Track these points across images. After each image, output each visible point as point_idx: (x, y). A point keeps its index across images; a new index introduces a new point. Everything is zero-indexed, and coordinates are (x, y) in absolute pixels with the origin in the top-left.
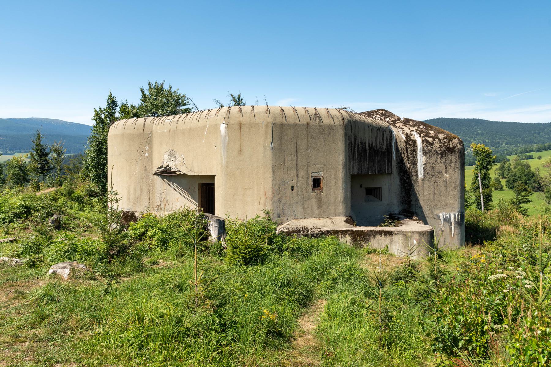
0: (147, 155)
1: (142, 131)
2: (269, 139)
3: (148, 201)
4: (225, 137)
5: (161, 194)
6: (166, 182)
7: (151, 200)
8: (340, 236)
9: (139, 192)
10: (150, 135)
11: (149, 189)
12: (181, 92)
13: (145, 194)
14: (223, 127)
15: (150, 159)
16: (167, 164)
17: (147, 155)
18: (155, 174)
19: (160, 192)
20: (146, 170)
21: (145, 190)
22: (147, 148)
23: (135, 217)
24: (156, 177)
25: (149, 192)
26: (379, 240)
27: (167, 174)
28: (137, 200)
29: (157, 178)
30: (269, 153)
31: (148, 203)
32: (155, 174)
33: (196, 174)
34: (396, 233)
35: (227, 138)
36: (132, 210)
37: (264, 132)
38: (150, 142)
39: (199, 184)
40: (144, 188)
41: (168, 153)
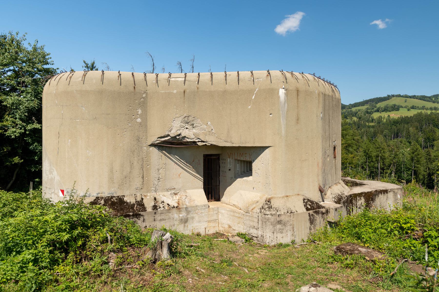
0: (139, 120)
1: (132, 89)
2: (321, 109)
3: (141, 180)
4: (285, 104)
5: (158, 170)
6: (165, 155)
7: (146, 179)
8: (358, 198)
9: (128, 169)
10: (144, 96)
11: (142, 165)
12: (46, 50)
13: (136, 172)
14: (282, 92)
15: (144, 125)
16: (179, 132)
17: (139, 120)
18: (152, 145)
19: (157, 167)
20: (138, 139)
21: (137, 166)
22: (140, 112)
23: (127, 203)
24: (152, 148)
25: (142, 168)
26: (380, 198)
27: (172, 145)
28: (126, 179)
29: (154, 150)
30: (320, 123)
31: (141, 183)
32: (152, 145)
33: (234, 145)
34: (389, 190)
35: (286, 105)
36: (119, 194)
37: (317, 101)
38: (144, 104)
39: (204, 155)
40: (135, 163)
41: (180, 119)
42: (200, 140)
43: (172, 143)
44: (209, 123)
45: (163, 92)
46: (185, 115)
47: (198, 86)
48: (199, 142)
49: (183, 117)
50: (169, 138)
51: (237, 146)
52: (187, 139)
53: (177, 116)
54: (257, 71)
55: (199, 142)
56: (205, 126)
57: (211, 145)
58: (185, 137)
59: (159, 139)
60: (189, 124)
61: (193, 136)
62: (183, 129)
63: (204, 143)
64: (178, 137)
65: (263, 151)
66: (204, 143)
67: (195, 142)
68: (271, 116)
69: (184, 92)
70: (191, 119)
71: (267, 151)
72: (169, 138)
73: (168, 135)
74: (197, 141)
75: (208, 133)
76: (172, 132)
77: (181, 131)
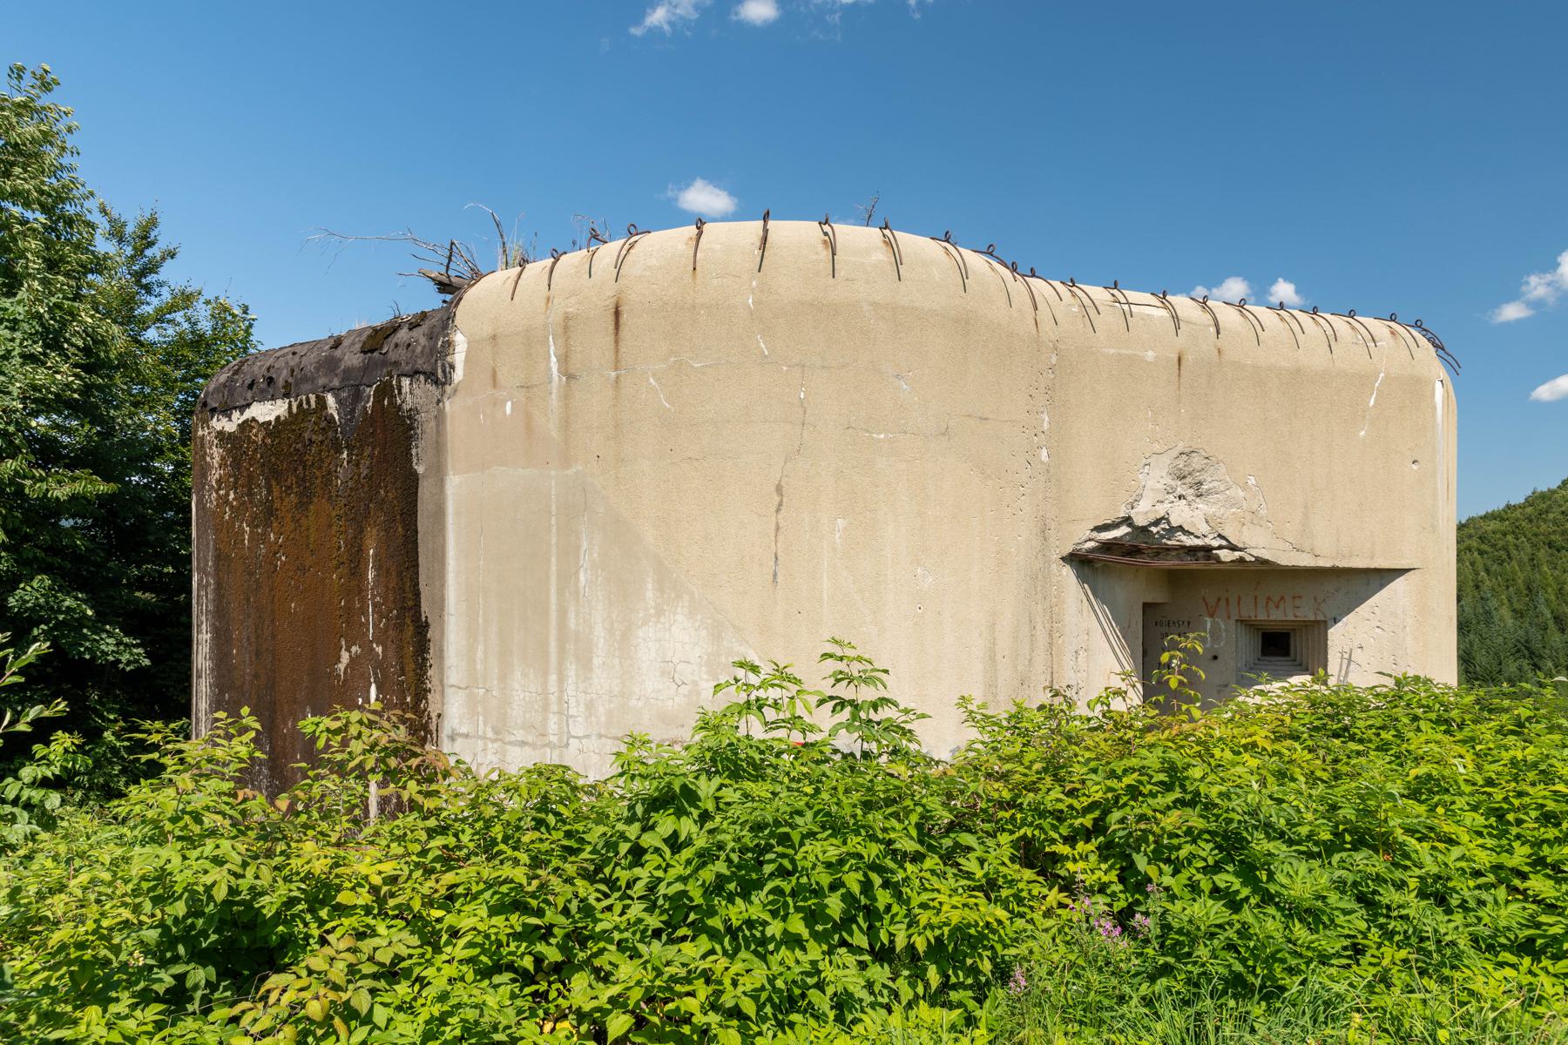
16: (1161, 511)
33: (1321, 563)
41: (1166, 460)
42: (1224, 543)
43: (1133, 551)
44: (1252, 481)
45: (1112, 351)
46: (1180, 448)
47: (1219, 343)
48: (1220, 547)
49: (1175, 453)
50: (1124, 530)
51: (1328, 565)
52: (1184, 538)
53: (1157, 447)
54: (844, 227)
55: (1220, 547)
56: (1241, 494)
57: (1261, 561)
58: (1181, 528)
59: (1095, 534)
60: (1188, 480)
61: (1203, 528)
62: (1171, 497)
63: (1237, 554)
64: (1154, 530)
65: (1382, 586)
66: (1237, 554)
67: (1207, 549)
68: (1415, 467)
69: (617, 314)
70: (1197, 461)
71: (1399, 584)
72: (1124, 530)
73: (1127, 520)
74: (1215, 543)
75: (1249, 516)
76: (1144, 506)
77: (1167, 506)
